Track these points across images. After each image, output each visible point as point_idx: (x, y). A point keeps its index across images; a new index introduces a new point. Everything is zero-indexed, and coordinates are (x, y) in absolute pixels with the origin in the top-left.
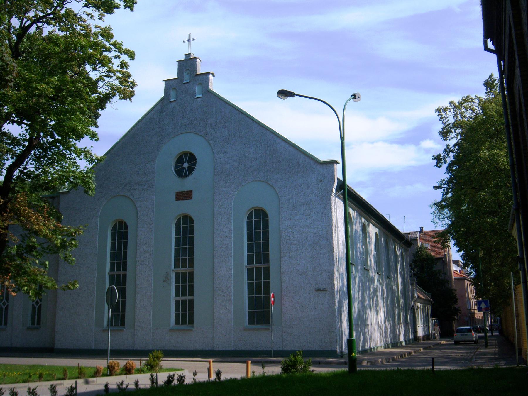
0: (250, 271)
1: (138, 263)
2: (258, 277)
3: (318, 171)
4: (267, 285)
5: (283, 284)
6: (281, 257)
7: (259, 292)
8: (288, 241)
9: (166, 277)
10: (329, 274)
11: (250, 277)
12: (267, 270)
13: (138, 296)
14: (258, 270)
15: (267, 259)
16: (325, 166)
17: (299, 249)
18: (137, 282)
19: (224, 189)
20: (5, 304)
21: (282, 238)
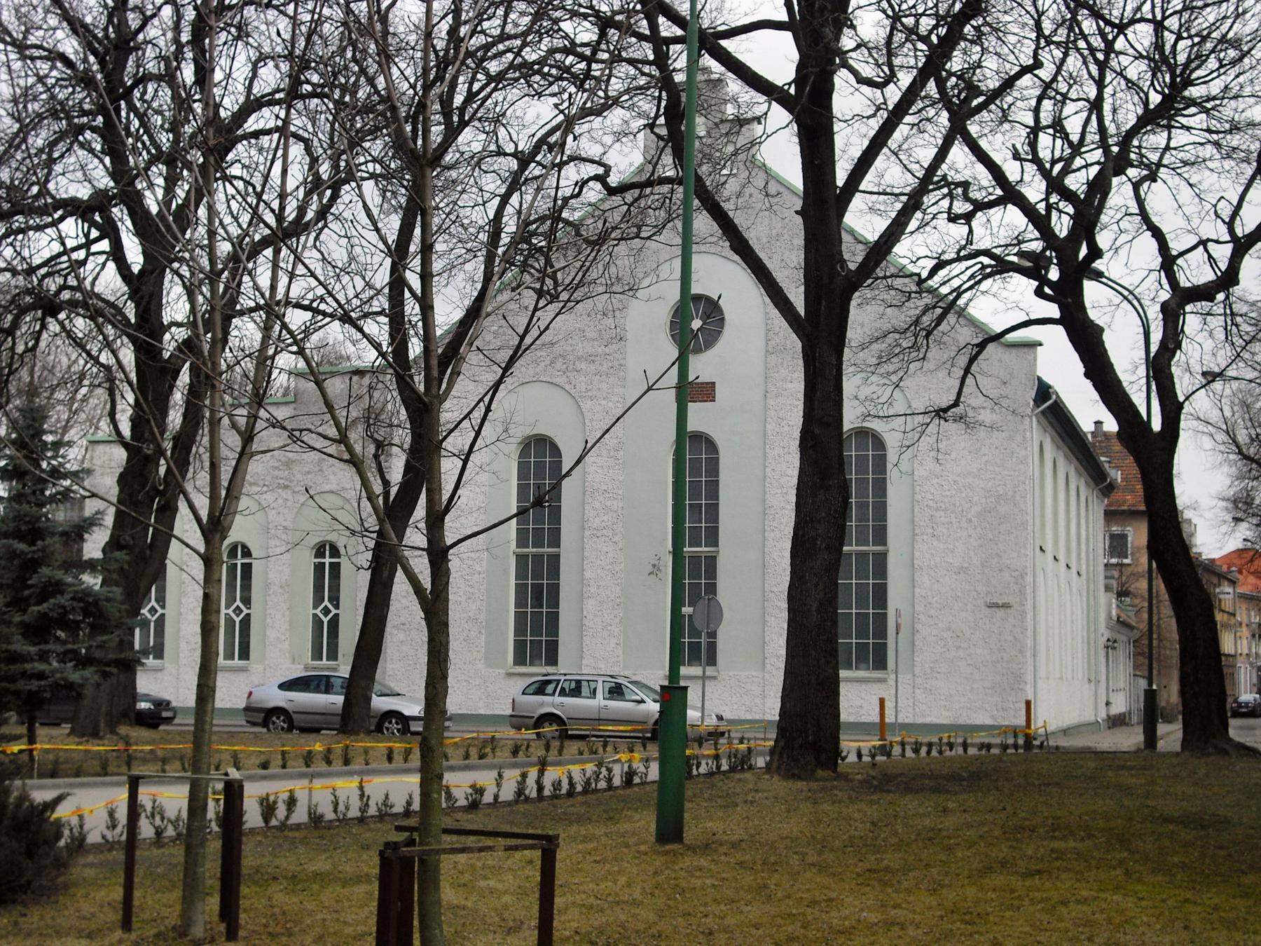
0: (521, 559)
1: (587, 533)
2: (537, 574)
3: (1000, 361)
4: (555, 590)
5: (917, 590)
6: (914, 535)
7: (538, 601)
8: (931, 503)
9: (654, 566)
10: (1016, 574)
11: (521, 573)
12: (555, 560)
13: (590, 605)
14: (538, 558)
15: (555, 540)
16: (1014, 351)
17: (953, 520)
18: (587, 574)
19: (789, 385)
20: (234, 611)
21: (918, 497)
